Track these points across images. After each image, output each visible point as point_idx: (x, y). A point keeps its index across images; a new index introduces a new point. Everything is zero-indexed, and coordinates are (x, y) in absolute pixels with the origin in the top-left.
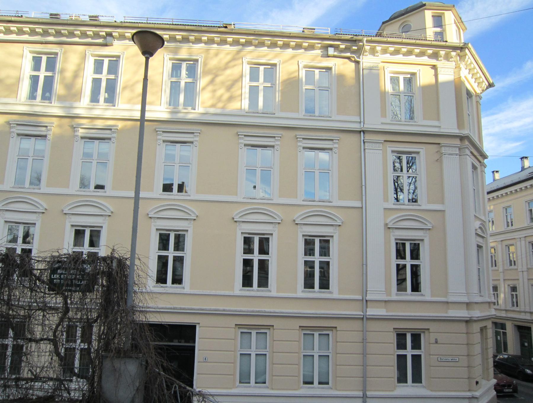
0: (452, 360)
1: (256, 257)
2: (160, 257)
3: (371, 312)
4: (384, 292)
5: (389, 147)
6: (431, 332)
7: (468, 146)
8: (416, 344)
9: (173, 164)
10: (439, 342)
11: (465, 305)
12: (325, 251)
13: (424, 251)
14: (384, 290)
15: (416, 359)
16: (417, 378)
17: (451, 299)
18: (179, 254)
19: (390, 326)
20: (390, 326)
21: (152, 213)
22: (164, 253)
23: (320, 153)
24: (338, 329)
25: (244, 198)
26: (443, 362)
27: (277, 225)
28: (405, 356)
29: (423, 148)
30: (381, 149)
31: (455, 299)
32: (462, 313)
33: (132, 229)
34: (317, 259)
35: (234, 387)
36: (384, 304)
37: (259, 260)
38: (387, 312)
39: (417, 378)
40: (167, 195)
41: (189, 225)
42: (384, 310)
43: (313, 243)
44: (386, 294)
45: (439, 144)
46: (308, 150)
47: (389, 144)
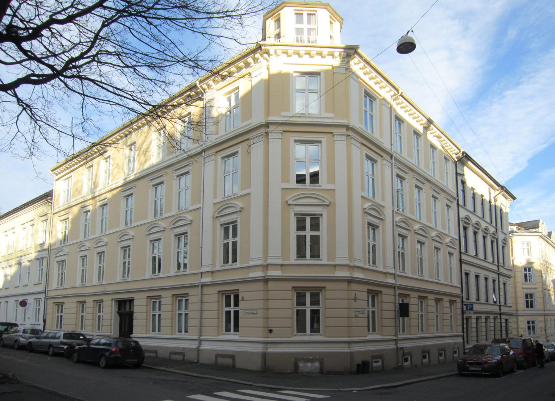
0: (252, 312)
1: (308, 233)
2: (298, 237)
3: (272, 273)
4: (280, 258)
5: (292, 137)
6: (327, 290)
7: (353, 137)
8: (315, 301)
9: (304, 161)
10: (244, 299)
11: (280, 266)
12: (315, 226)
13: (323, 223)
14: (280, 256)
15: (237, 313)
16: (315, 329)
17: (337, 262)
18: (302, 233)
19: (289, 285)
20: (289, 285)
21: (291, 201)
22: (315, 233)
23: (310, 146)
24: (326, 289)
25: (71, 176)
26: (246, 315)
27: (326, 207)
28: (230, 312)
29: (324, 138)
30: (281, 138)
31: (357, 264)
32: (259, 274)
33: (347, 215)
34: (308, 233)
35: (293, 335)
36: (280, 267)
37: (311, 236)
38: (282, 273)
39: (315, 329)
40: (300, 186)
41: (323, 210)
42: (280, 272)
43: (305, 220)
44: (281, 259)
45: (332, 133)
46: (299, 144)
47: (291, 135)
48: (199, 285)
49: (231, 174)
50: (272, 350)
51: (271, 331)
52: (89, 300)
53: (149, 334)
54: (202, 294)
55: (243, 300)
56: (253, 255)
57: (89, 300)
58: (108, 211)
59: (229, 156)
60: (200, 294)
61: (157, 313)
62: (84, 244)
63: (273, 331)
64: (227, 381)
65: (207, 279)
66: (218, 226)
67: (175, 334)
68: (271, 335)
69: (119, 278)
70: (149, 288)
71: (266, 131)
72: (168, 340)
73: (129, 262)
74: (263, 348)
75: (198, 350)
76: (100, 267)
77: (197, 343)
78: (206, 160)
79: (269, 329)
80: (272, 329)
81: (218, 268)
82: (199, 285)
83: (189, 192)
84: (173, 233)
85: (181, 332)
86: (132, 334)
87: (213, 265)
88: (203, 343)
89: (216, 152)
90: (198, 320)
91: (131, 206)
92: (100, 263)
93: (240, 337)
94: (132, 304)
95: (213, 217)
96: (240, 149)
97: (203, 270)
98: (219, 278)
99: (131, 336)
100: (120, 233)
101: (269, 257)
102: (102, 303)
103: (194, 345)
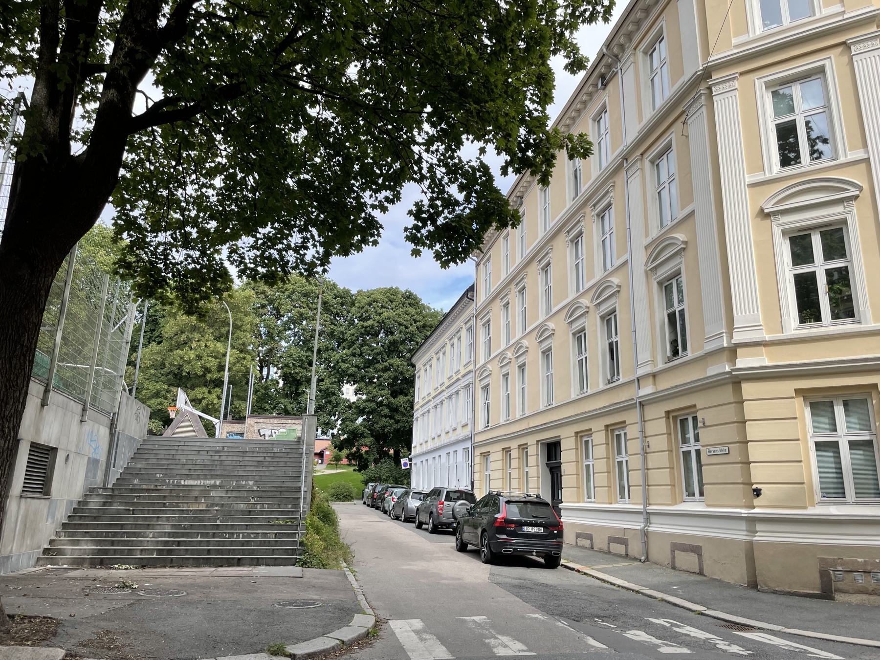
0: (721, 451)
48: (636, 403)
49: (666, 185)
50: (764, 536)
51: (758, 493)
52: (598, 426)
53: (584, 502)
54: (644, 421)
55: (704, 426)
56: (644, 356)
57: (598, 426)
58: (613, 225)
59: (660, 155)
60: (639, 420)
61: (692, 447)
62: (579, 302)
63: (762, 492)
64: (663, 600)
65: (647, 390)
66: (655, 286)
67: (615, 503)
68: (756, 501)
69: (574, 394)
70: (575, 416)
71: (708, 86)
72: (583, 512)
73: (586, 358)
74: (747, 531)
75: (646, 534)
76: (580, 361)
77: (643, 521)
78: (630, 173)
79: (754, 487)
80: (759, 486)
81: (661, 366)
82: (636, 403)
83: (674, 187)
84: (655, 279)
85: (694, 495)
86: (562, 502)
87: (653, 361)
88: (653, 519)
89: (642, 154)
90: (640, 472)
91: (582, 255)
92: (580, 352)
93: (708, 506)
94: (558, 448)
95: (646, 272)
96: (673, 136)
97: (641, 372)
98: (666, 384)
99: (560, 506)
100: (594, 290)
101: (735, 330)
102: (590, 439)
103: (637, 524)
